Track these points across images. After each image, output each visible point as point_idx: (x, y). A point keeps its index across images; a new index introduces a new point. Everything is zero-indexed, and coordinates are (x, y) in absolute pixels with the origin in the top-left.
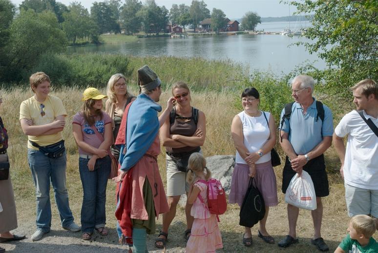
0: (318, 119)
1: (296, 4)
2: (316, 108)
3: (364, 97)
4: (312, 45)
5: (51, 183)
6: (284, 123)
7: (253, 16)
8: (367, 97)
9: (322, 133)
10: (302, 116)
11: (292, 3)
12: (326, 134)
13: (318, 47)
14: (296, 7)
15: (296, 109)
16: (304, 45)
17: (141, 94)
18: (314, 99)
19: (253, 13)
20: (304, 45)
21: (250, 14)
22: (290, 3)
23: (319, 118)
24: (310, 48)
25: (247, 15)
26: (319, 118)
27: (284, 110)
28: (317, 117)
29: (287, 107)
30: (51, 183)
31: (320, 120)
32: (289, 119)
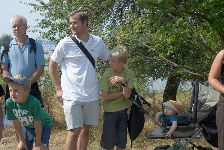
0: (31, 51)
1: (33, 5)
2: (29, 43)
3: (80, 22)
4: (45, 33)
5: (128, 130)
6: (3, 57)
7: (8, 38)
8: (82, 23)
9: (35, 63)
10: (18, 50)
11: (30, 4)
12: (39, 63)
13: (49, 34)
14: (33, 7)
15: (13, 45)
16: (38, 32)
17: (17, 103)
18: (27, 36)
19: (8, 35)
20: (38, 32)
21: (6, 36)
22: (29, 4)
23: (32, 50)
24: (43, 35)
25: (3, 36)
26: (32, 50)
27: (3, 47)
28: (31, 50)
29: (5, 44)
30: (128, 130)
31: (33, 52)
32: (7, 54)
